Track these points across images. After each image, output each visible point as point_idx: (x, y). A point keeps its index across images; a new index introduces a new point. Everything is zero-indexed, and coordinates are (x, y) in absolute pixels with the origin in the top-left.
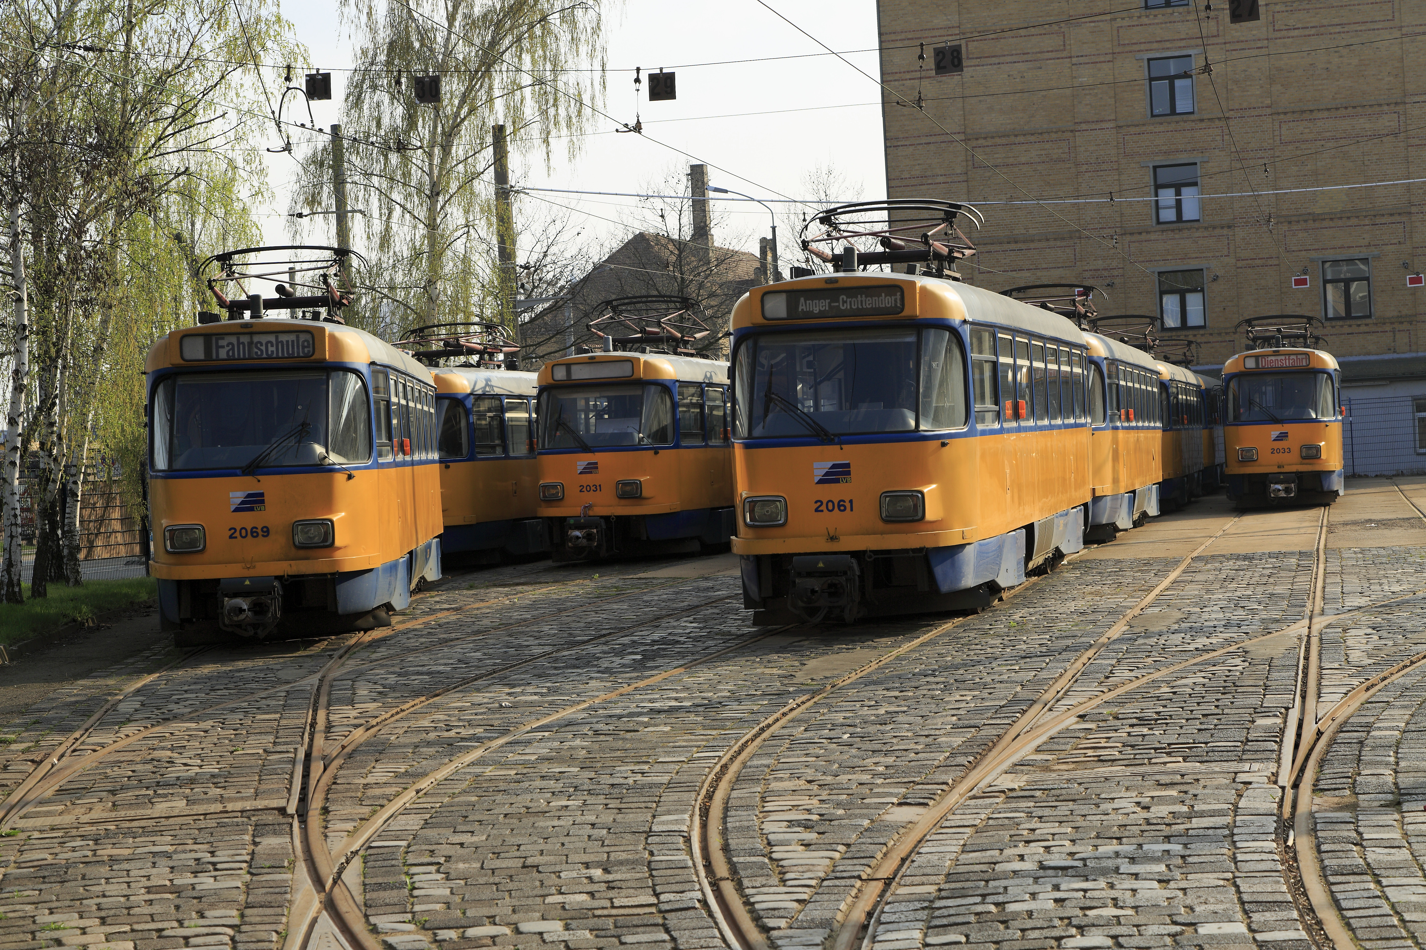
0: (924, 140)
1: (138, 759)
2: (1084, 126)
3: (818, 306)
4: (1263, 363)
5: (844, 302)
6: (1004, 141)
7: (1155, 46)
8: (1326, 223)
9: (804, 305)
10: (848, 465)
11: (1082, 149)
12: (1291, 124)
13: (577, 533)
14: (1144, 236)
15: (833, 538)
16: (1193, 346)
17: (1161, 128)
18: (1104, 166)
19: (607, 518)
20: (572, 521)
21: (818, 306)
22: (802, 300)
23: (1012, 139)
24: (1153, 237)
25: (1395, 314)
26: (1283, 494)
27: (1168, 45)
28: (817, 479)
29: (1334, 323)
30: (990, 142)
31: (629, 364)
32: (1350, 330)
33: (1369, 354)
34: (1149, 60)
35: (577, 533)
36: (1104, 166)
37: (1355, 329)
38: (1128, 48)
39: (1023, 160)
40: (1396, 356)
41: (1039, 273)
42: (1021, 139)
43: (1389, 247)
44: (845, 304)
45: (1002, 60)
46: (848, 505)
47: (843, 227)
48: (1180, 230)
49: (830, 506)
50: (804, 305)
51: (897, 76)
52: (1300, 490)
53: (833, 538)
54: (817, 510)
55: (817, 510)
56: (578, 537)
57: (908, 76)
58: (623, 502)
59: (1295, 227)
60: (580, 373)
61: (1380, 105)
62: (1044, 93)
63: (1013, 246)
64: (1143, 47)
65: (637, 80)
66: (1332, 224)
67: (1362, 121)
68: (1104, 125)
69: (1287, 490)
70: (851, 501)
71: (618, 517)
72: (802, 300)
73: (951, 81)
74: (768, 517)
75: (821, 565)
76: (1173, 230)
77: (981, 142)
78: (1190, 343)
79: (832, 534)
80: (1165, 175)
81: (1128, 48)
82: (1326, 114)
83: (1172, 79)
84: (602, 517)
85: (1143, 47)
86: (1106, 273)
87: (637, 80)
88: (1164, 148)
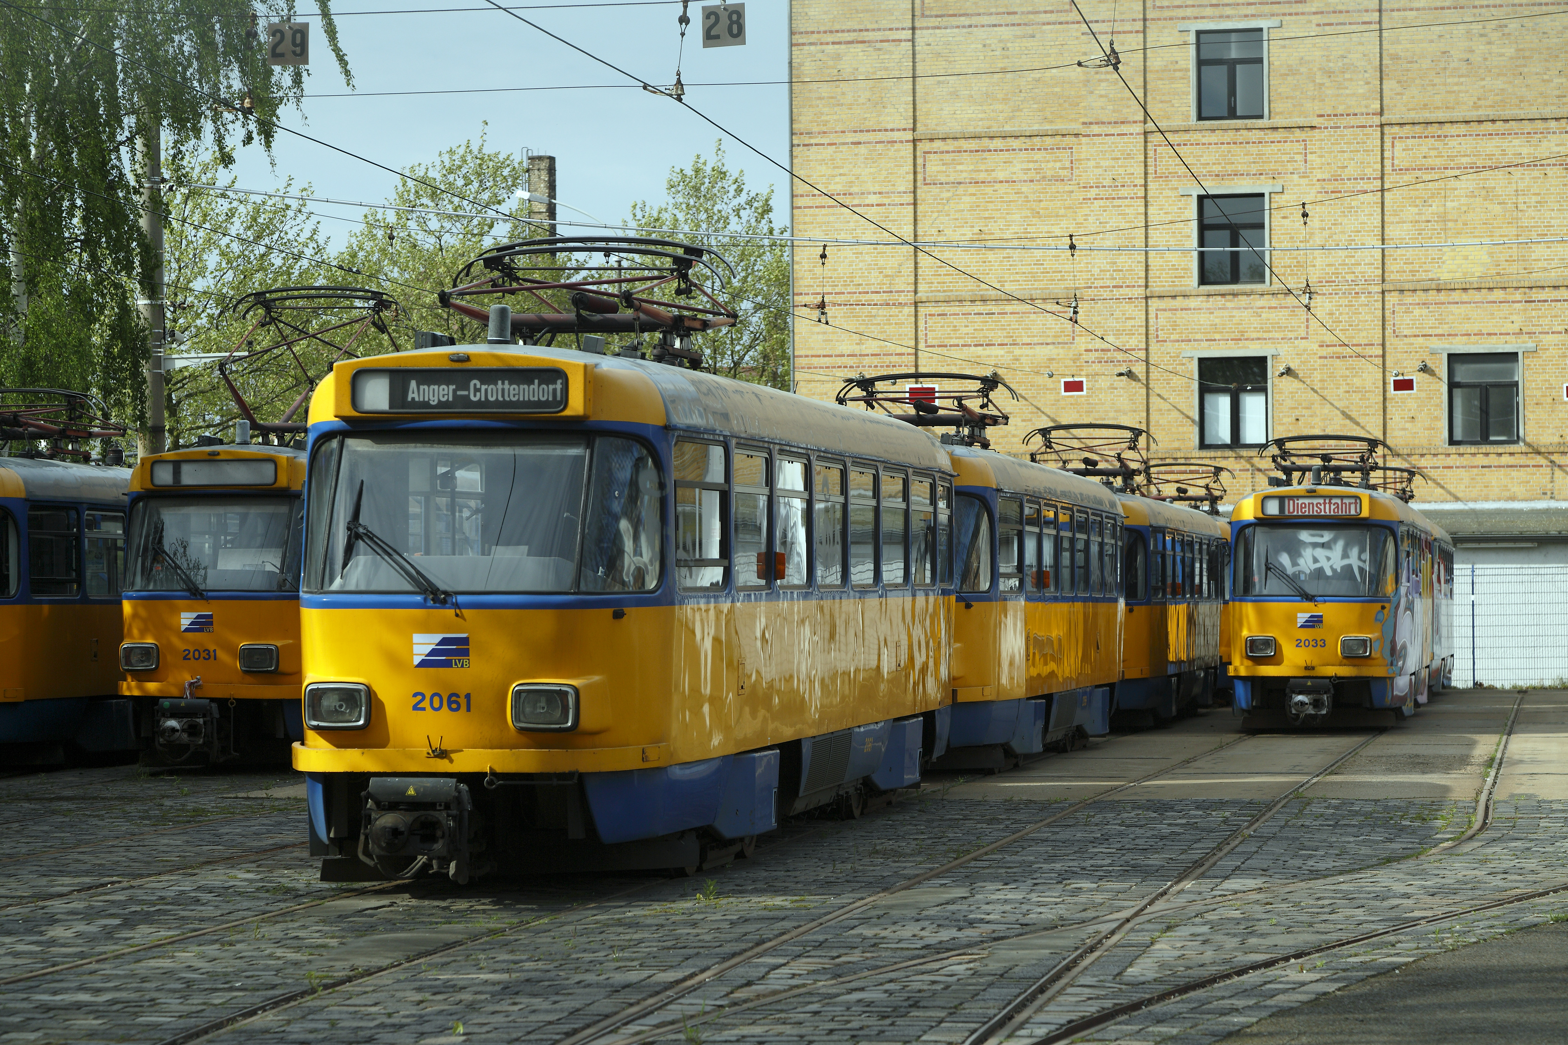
0: (851, 138)
1: (1423, 926)
2: (1096, 129)
3: (437, 394)
4: (1290, 508)
5: (477, 390)
6: (973, 144)
7: (1209, 11)
8: (1456, 296)
9: (415, 392)
10: (465, 641)
11: (1092, 163)
12: (1410, 142)
13: (172, 723)
14: (1179, 302)
15: (442, 754)
16: (1224, 475)
17: (1213, 138)
18: (1124, 192)
19: (222, 703)
20: (166, 703)
21: (437, 394)
22: (413, 384)
23: (986, 142)
24: (1193, 303)
25: (1556, 439)
26: (1311, 711)
27: (1228, 11)
28: (417, 660)
29: (1462, 449)
30: (951, 145)
31: (270, 467)
32: (1485, 461)
33: (1513, 499)
34: (1199, 33)
35: (172, 723)
36: (1124, 192)
37: (1493, 460)
38: (1167, 13)
39: (1001, 176)
40: (1553, 504)
41: (1017, 351)
42: (998, 143)
43: (1550, 337)
44: (479, 392)
45: (974, 20)
46: (463, 701)
47: (520, 274)
48: (1235, 295)
49: (436, 704)
50: (415, 392)
51: (814, 38)
52: (1337, 703)
53: (442, 754)
54: (416, 708)
55: (416, 708)
56: (173, 730)
57: (830, 38)
58: (249, 679)
59: (1409, 300)
60: (191, 476)
61: (1545, 119)
62: (1037, 75)
63: (979, 308)
64: (1189, 12)
65: (684, 20)
66: (1465, 297)
67: (1516, 142)
68: (1124, 129)
69: (1316, 704)
70: (468, 696)
71: (240, 701)
72: (413, 384)
73: (725, 55)
74: (356, 714)
75: (411, 792)
76: (1223, 295)
77: (937, 145)
78: (1218, 470)
79: (436, 744)
80: (1212, 213)
81: (1167, 13)
82: (1462, 129)
83: (1231, 64)
84: (212, 700)
85: (1189, 12)
86: (1120, 356)
87: (684, 20)
88: (1216, 169)
